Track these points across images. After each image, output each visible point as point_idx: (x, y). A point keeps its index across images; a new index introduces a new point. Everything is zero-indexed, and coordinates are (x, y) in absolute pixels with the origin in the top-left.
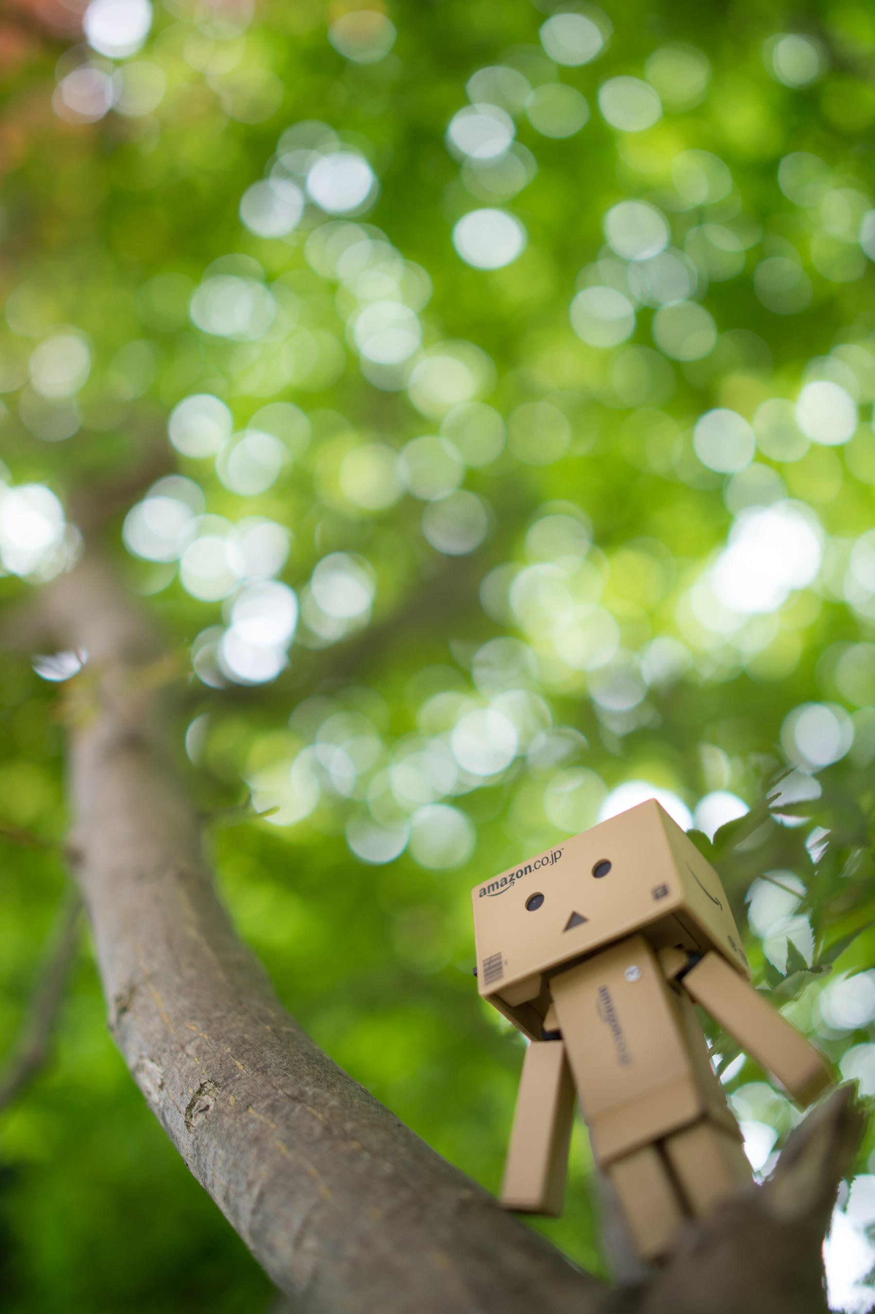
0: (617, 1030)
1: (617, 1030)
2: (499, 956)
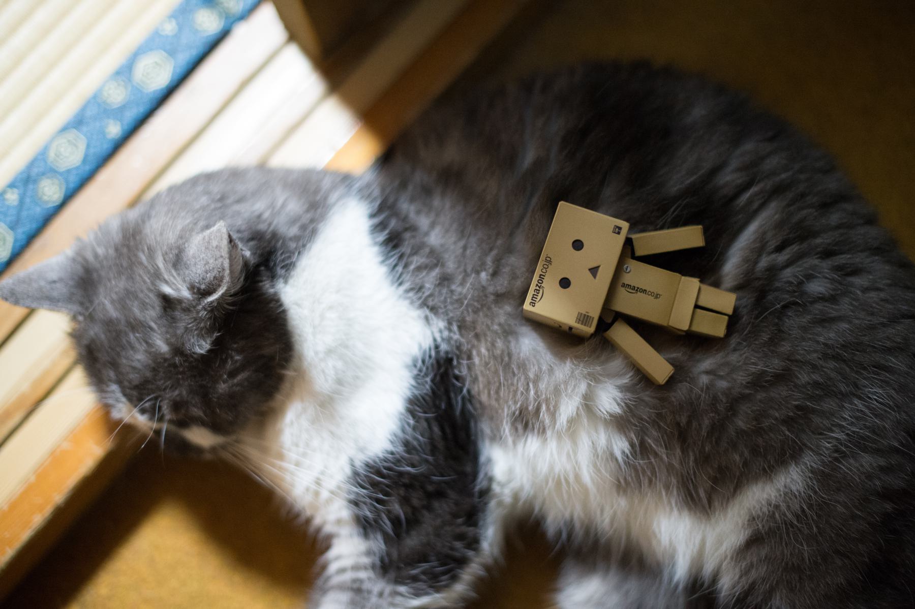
0: (644, 291)
1: (644, 291)
2: (580, 314)
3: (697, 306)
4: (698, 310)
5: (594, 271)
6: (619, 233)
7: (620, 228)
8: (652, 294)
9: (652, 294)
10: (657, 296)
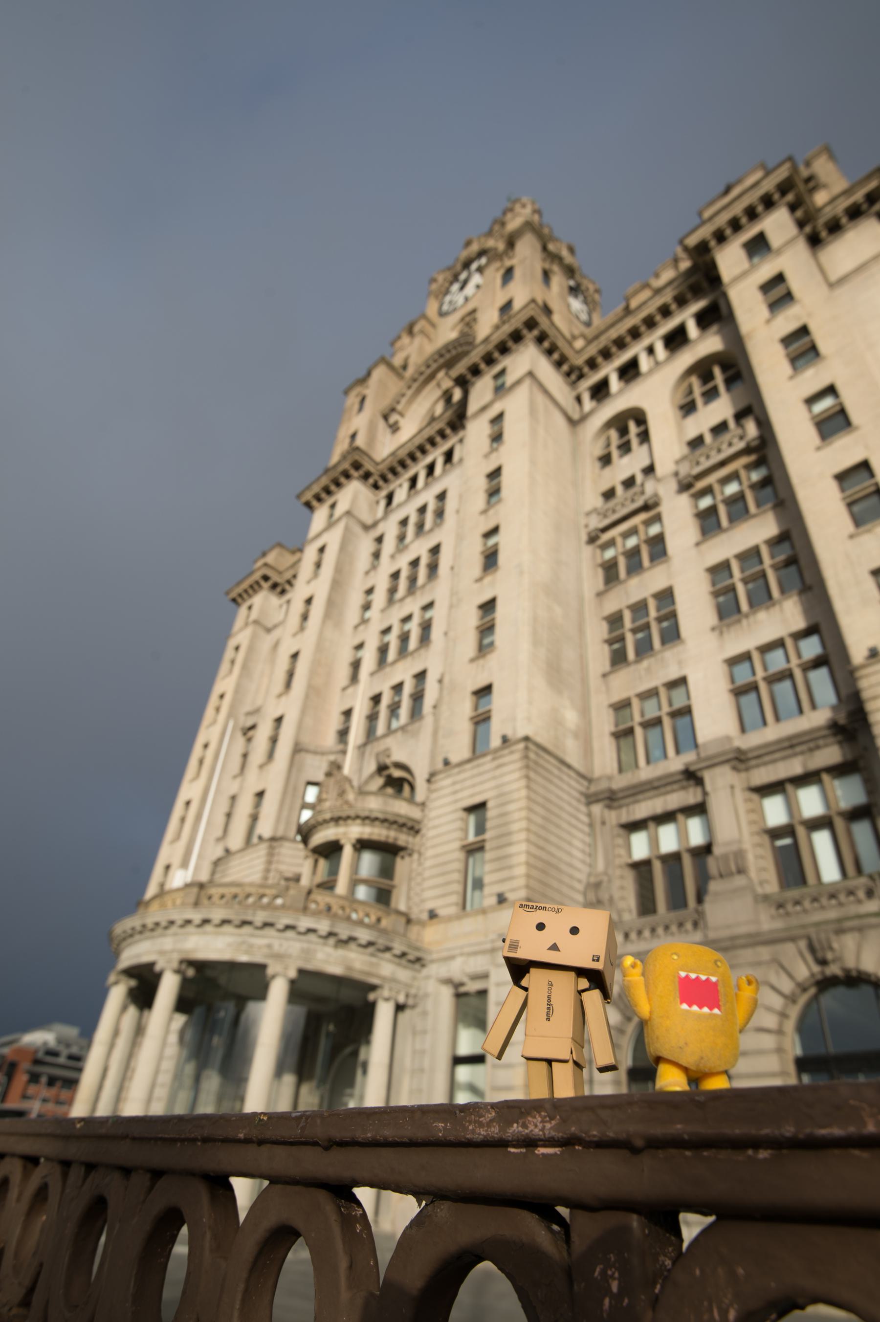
0: (549, 997)
1: (549, 997)
3: (549, 1062)
4: (527, 383)
5: (554, 947)
6: (593, 960)
7: (598, 960)
8: (550, 990)
9: (550, 990)
10: (550, 984)
